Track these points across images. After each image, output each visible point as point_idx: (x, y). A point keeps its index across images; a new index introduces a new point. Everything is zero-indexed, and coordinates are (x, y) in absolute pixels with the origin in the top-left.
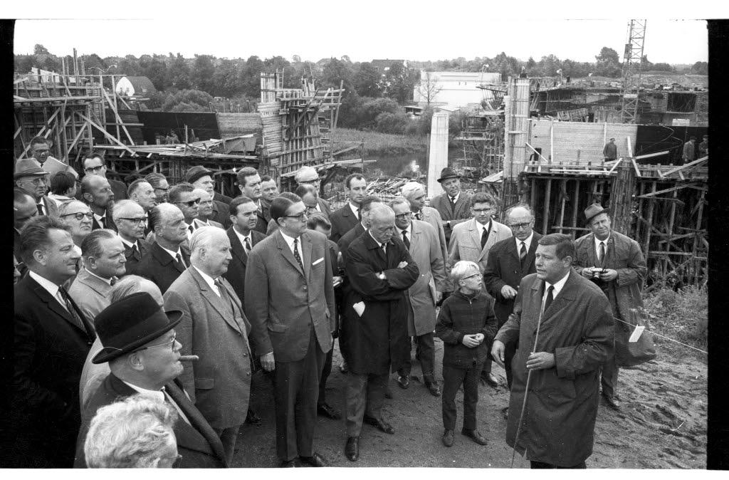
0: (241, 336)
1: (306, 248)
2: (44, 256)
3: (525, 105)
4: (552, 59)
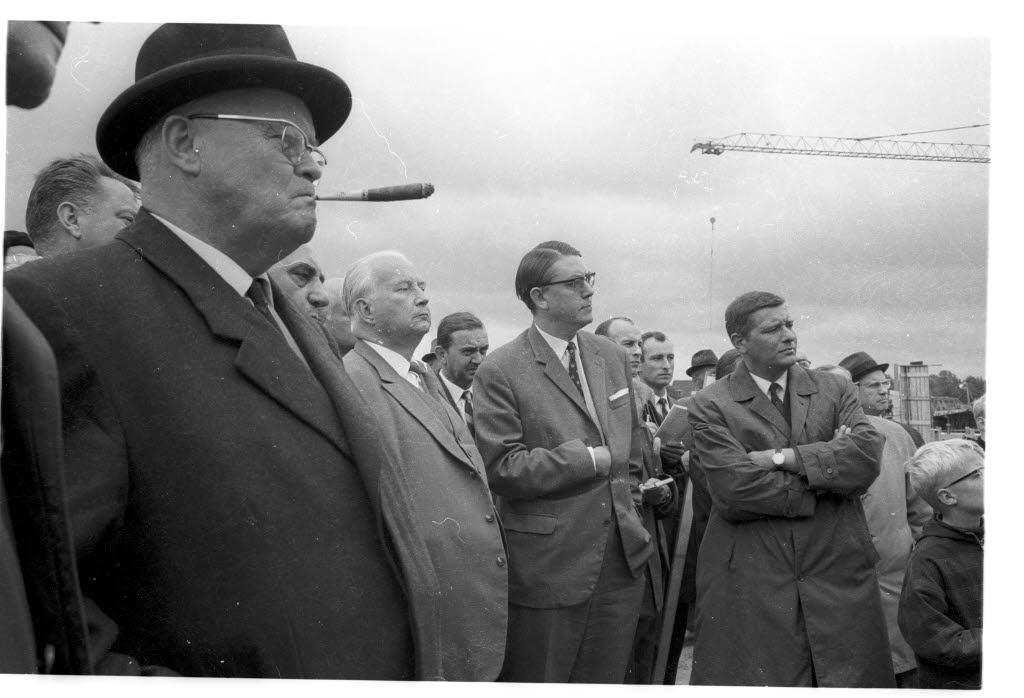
0: (475, 476)
1: (592, 367)
2: (80, 220)
3: (925, 407)
4: (945, 379)
